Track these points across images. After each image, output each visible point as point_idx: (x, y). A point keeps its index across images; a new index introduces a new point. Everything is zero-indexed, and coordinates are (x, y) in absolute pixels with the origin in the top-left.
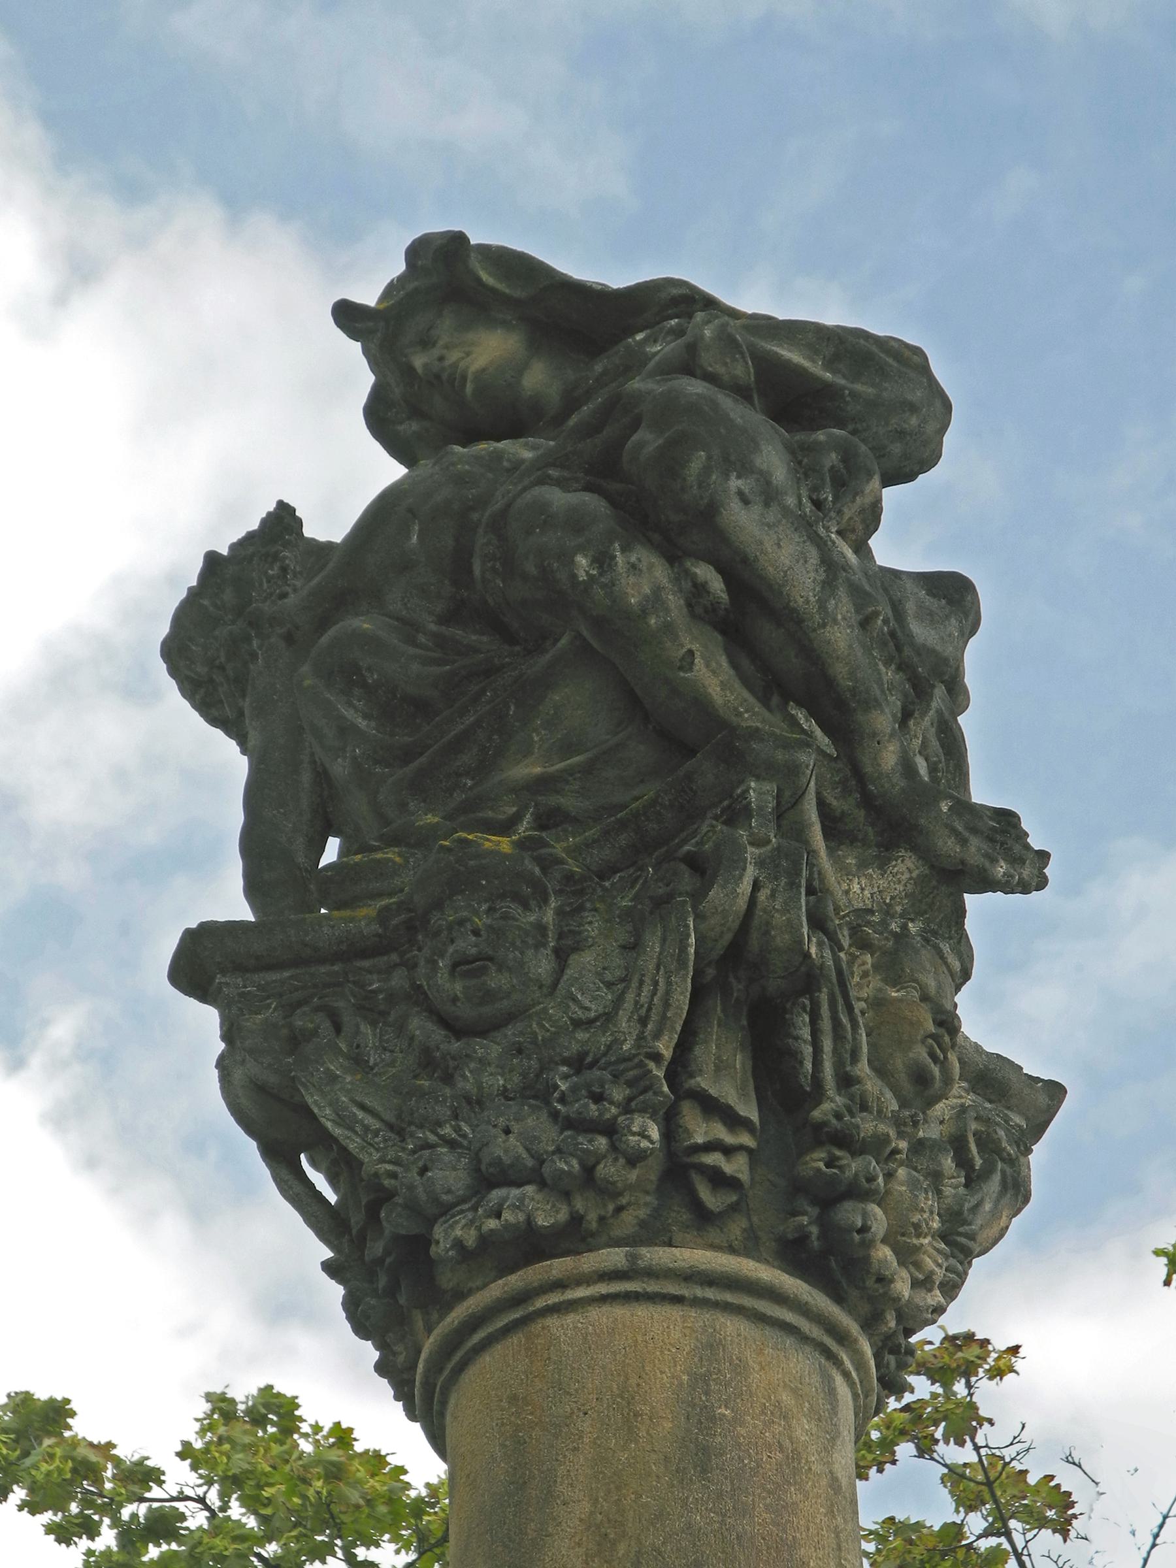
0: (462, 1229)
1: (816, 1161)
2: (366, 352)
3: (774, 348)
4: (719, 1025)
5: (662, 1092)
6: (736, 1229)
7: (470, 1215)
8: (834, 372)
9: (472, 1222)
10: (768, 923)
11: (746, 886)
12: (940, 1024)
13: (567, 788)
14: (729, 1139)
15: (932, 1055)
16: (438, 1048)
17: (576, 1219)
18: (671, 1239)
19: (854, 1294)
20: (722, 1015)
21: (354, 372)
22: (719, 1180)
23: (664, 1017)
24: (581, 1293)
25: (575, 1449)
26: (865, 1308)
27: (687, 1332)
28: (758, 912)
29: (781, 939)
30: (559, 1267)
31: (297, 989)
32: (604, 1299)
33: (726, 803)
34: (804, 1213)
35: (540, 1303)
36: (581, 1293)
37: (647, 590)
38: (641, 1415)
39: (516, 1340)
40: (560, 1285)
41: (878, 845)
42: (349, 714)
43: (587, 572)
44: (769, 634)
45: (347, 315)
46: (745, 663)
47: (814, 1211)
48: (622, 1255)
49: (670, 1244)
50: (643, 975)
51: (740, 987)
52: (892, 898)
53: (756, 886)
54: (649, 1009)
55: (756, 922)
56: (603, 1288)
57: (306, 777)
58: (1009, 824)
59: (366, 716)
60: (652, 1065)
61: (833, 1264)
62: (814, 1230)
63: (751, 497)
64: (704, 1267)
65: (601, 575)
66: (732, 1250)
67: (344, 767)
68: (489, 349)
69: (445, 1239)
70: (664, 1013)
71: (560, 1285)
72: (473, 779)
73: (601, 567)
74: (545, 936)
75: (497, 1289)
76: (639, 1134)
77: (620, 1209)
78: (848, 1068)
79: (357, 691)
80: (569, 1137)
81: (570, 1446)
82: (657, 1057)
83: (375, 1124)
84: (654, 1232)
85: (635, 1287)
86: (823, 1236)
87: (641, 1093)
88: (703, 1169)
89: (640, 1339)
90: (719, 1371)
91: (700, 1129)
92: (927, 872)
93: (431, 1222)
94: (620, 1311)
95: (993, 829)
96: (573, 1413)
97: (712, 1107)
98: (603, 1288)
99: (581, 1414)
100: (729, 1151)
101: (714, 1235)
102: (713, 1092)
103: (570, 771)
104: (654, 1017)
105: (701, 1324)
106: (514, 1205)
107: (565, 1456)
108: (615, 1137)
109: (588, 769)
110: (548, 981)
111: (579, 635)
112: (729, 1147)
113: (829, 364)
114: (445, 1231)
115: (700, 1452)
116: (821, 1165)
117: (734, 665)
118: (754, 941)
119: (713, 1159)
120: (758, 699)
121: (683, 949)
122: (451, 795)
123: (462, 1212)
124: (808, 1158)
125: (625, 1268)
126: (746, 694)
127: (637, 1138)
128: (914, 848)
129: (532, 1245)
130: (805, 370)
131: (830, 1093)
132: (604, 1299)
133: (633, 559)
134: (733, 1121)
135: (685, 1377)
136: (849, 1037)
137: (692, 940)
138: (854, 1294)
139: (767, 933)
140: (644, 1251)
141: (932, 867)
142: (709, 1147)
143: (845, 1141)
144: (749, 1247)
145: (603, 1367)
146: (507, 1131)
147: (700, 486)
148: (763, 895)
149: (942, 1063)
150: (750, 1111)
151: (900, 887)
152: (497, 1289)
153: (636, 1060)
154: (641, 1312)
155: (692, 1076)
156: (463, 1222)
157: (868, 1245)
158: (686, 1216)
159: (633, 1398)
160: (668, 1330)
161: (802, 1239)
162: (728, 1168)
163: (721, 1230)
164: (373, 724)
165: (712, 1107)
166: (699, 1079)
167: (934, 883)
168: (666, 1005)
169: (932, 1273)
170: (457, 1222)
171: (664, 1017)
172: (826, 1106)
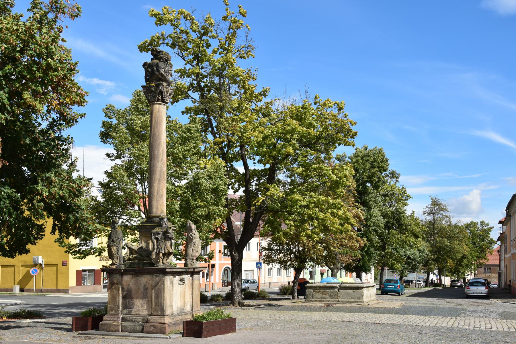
115: (159, 111)
160: (157, 105)
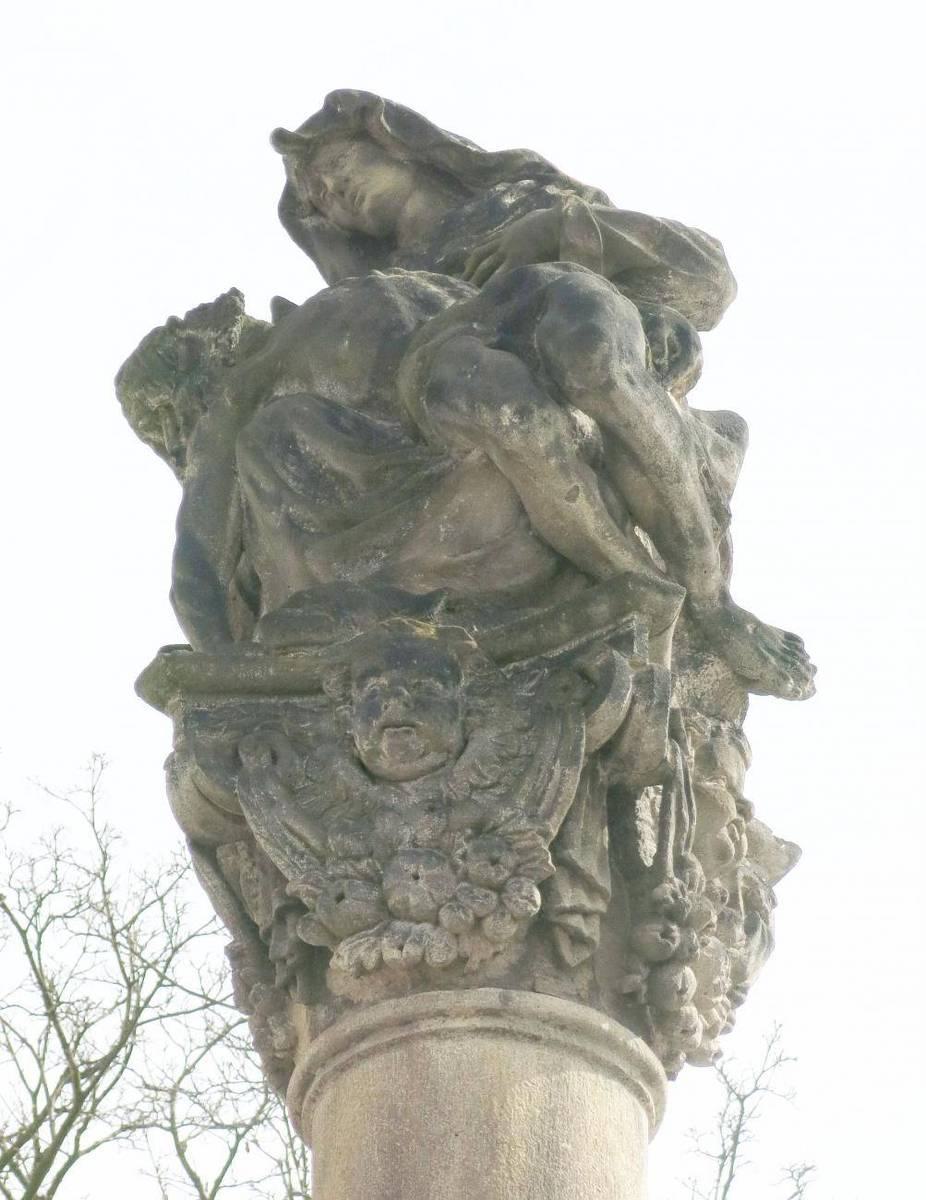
0: (365, 950)
1: (654, 930)
2: (285, 160)
3: (620, 233)
4: (588, 805)
5: (548, 865)
6: (583, 979)
7: (372, 939)
8: (660, 254)
9: (374, 945)
10: (639, 731)
11: (627, 702)
12: (741, 811)
13: (464, 573)
14: (588, 905)
15: (732, 836)
16: (358, 790)
17: (462, 960)
18: (534, 985)
19: (659, 1036)
20: (590, 797)
21: (273, 174)
22: (578, 939)
23: (555, 801)
24: (459, 1023)
25: (446, 1168)
26: (664, 1048)
27: (540, 1068)
28: (633, 722)
29: (648, 746)
30: (444, 999)
31: (243, 716)
32: (477, 1031)
33: (611, 627)
34: (638, 972)
35: (424, 1027)
36: (459, 1023)
37: (552, 438)
38: (502, 1143)
39: (398, 1054)
40: (442, 1014)
41: (691, 647)
42: (283, 474)
43: (510, 420)
44: (633, 479)
45: (281, 139)
46: (612, 498)
47: (645, 971)
48: (497, 995)
49: (533, 990)
50: (541, 764)
51: (605, 774)
52: (703, 694)
53: (634, 700)
54: (544, 792)
55: (630, 730)
56: (477, 1022)
57: (233, 512)
58: (796, 648)
59: (295, 478)
60: (541, 840)
61: (648, 1012)
62: (644, 988)
63: (635, 379)
64: (559, 1014)
65: (521, 423)
66: (579, 999)
67: (277, 520)
68: (382, 181)
69: (349, 958)
70: (556, 798)
71: (442, 1014)
72: (387, 552)
73: (521, 418)
74: (456, 711)
75: (388, 1009)
76: (527, 898)
77: (496, 954)
78: (683, 853)
79: (291, 458)
80: (466, 888)
81: (443, 1165)
82: (545, 834)
83: (300, 847)
84: (519, 976)
85: (500, 1025)
86: (650, 991)
87: (529, 861)
88: (565, 928)
89: (504, 1072)
90: (564, 1107)
91: (570, 896)
92: (730, 676)
93: (336, 940)
94: (488, 1045)
95: (784, 650)
96: (446, 1133)
97: (576, 875)
98: (477, 1022)
99: (453, 1135)
100: (586, 914)
101: (566, 985)
102: (581, 864)
103: (467, 562)
104: (547, 799)
105: (551, 1062)
106: (415, 940)
107: (438, 1173)
108: (504, 895)
109: (481, 563)
110: (455, 750)
111: (487, 455)
112: (584, 908)
113: (658, 250)
114: (351, 950)
116: (658, 935)
117: (602, 494)
118: (626, 744)
119: (576, 921)
120: (618, 526)
121: (577, 747)
122: (368, 562)
123: (366, 935)
124: (647, 927)
125: (498, 1008)
126: (611, 523)
127: (526, 901)
128: (722, 656)
129: (421, 976)
130: (640, 250)
131: (671, 874)
132: (477, 1031)
133: (546, 415)
134: (592, 888)
135: (538, 1111)
136: (687, 829)
137: (584, 741)
138: (659, 1036)
139: (637, 739)
140: (514, 993)
141: (734, 673)
142: (573, 911)
143: (674, 914)
144: (590, 998)
145: (473, 1094)
146: (416, 877)
147: (602, 368)
148: (639, 708)
149: (737, 843)
150: (605, 882)
151: (709, 686)
152: (388, 1009)
153: (530, 834)
154: (506, 1047)
155: (566, 848)
156: (366, 945)
157: (682, 1002)
158: (547, 965)
159: (496, 1126)
161: (632, 996)
162: (586, 931)
163: (572, 980)
164: (301, 486)
165: (576, 875)
166: (571, 851)
167: (733, 684)
168: (559, 792)
169: (718, 1022)
170: (360, 944)
171: (555, 801)
172: (668, 886)
